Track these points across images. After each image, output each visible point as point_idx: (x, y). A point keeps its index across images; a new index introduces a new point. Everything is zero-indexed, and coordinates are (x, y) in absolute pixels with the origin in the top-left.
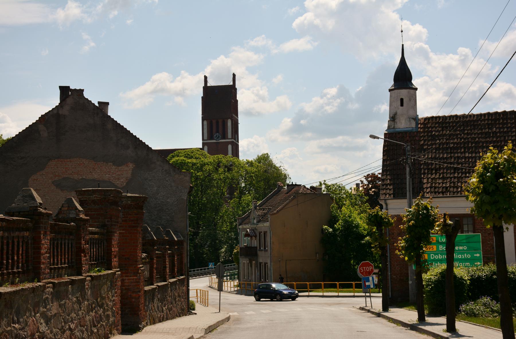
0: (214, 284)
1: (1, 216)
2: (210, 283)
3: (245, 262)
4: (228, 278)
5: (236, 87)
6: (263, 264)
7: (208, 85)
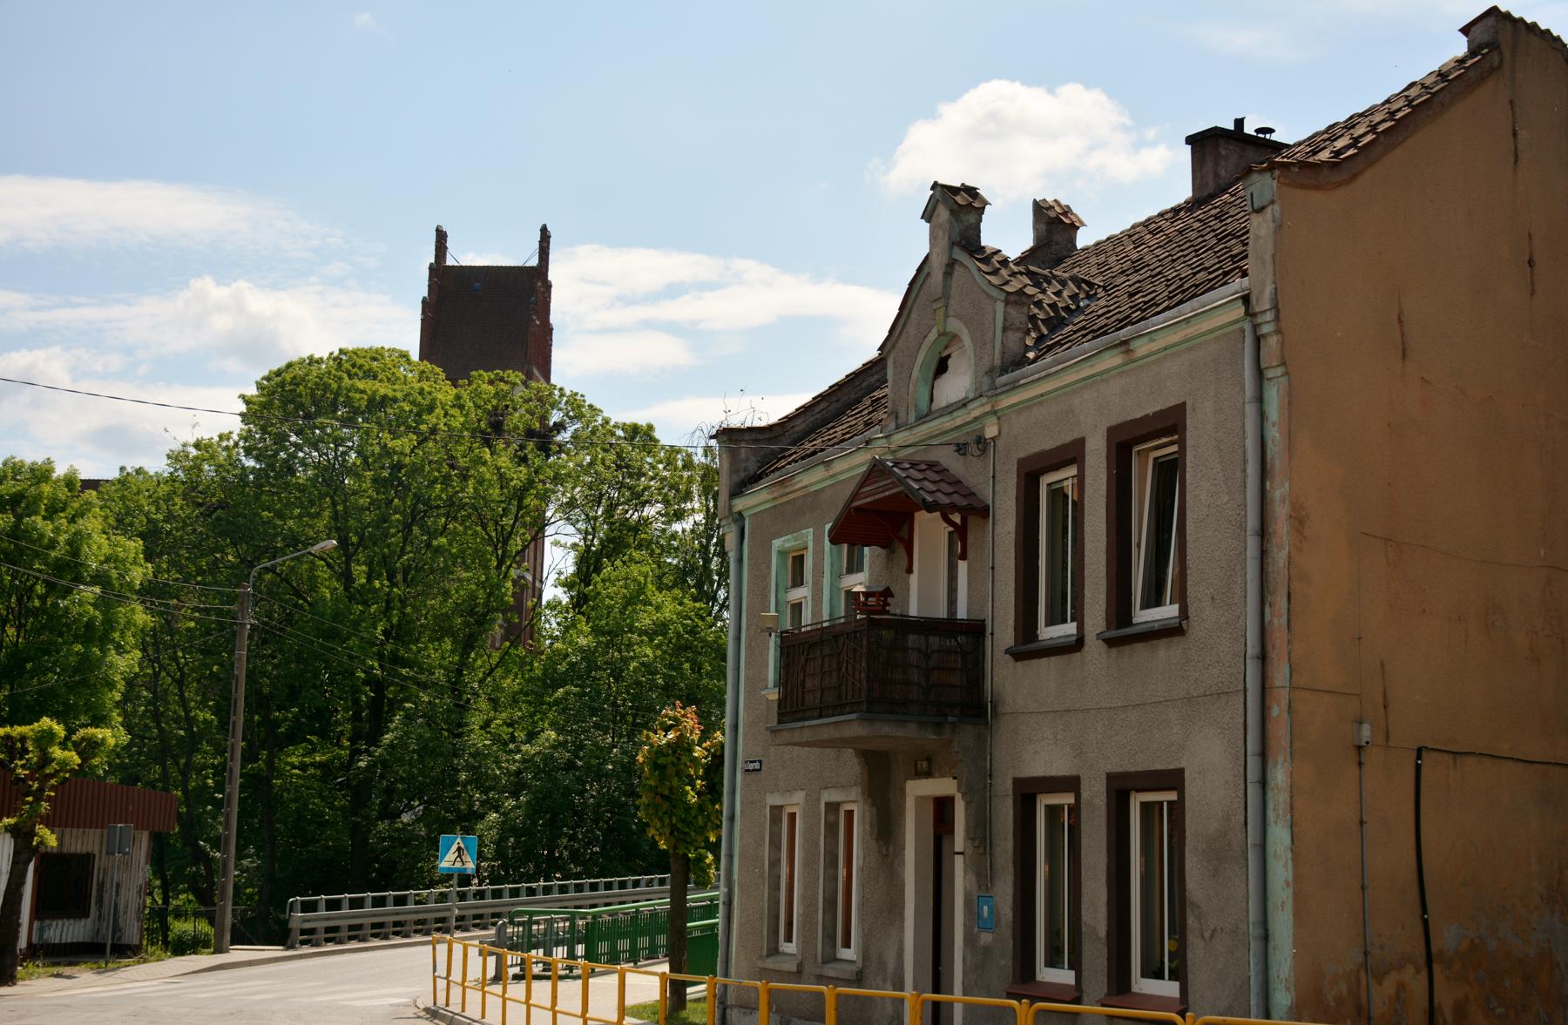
0: (456, 992)
1: (541, 1020)
2: (442, 984)
3: (795, 802)
4: (580, 949)
5: (551, 276)
6: (1095, 795)
7: (450, 262)
